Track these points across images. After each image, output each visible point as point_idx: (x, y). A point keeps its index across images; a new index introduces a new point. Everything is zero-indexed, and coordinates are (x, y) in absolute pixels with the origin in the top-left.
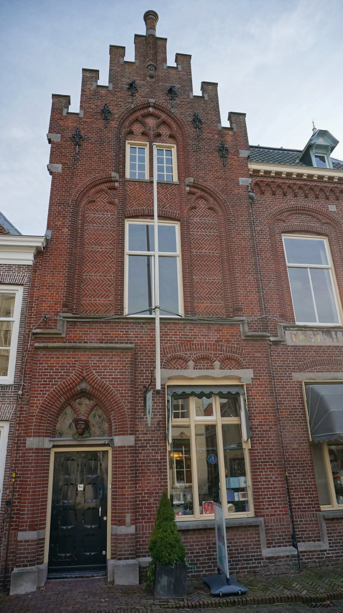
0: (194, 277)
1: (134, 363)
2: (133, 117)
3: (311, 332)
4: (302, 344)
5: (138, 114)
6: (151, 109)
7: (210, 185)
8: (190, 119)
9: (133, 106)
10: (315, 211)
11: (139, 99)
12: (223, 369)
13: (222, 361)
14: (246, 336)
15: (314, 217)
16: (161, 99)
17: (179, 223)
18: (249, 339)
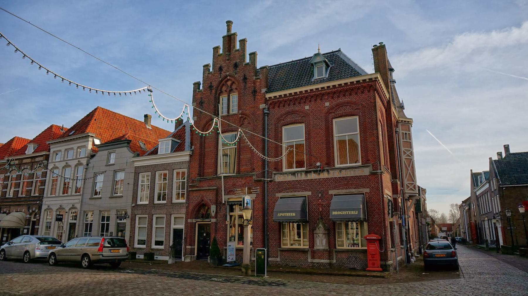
8: (242, 78)
11: (223, 74)
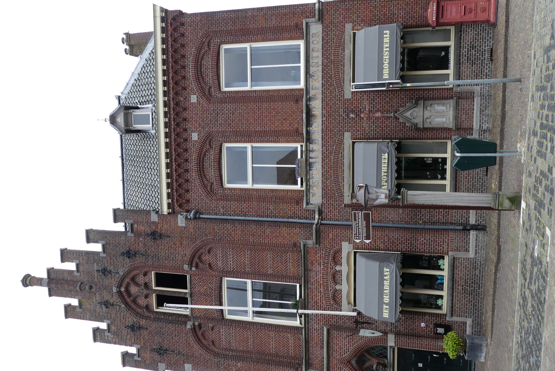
0: (269, 272)
1: (339, 328)
2: (132, 305)
3: (311, 180)
4: (320, 190)
5: (128, 300)
6: (123, 289)
7: (188, 252)
9: (123, 306)
10: (199, 50)
11: (116, 299)
12: (341, 264)
13: (336, 283)
14: (317, 244)
15: (205, 154)
16: (112, 282)
17: (223, 278)
18: (318, 241)
